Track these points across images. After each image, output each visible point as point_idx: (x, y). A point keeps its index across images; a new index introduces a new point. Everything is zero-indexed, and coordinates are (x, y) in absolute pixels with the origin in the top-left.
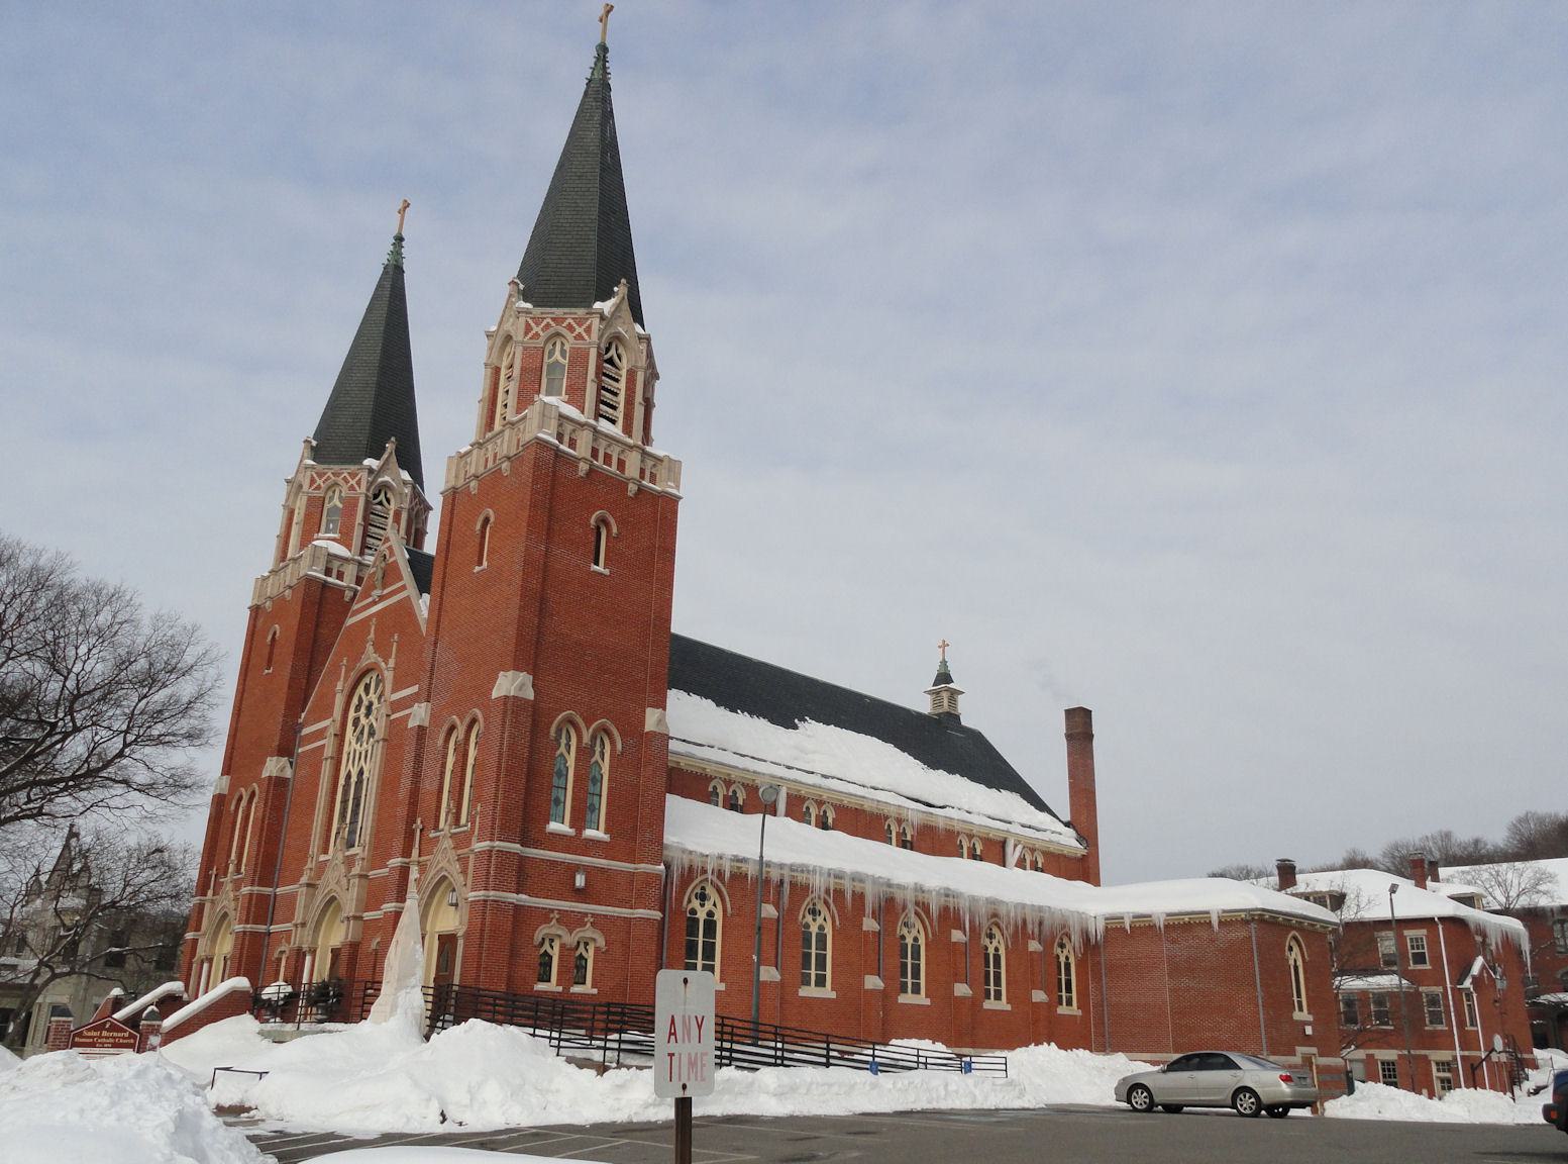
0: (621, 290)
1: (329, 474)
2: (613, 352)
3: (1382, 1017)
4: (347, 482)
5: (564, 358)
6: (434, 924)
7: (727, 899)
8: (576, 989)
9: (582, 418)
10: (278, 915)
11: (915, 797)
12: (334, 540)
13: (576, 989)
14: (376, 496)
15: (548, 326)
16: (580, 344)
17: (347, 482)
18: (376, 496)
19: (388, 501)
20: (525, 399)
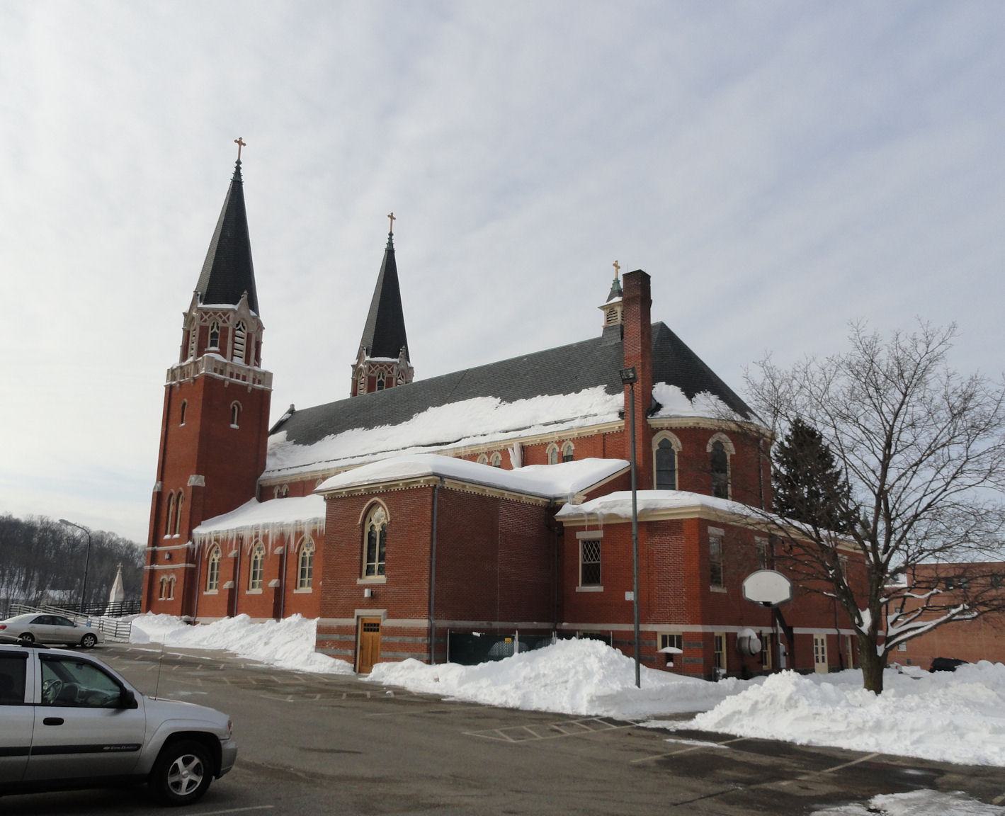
0: (245, 296)
1: (211, 313)
2: (240, 326)
3: (44, 621)
4: (221, 318)
5: (218, 330)
6: (284, 549)
7: (386, 509)
8: (168, 599)
9: (225, 361)
10: (182, 572)
11: (518, 427)
12: (215, 352)
13: (168, 599)
14: (237, 325)
15: (211, 316)
16: (224, 325)
17: (221, 318)
18: (237, 325)
19: (244, 328)
20: (200, 352)
